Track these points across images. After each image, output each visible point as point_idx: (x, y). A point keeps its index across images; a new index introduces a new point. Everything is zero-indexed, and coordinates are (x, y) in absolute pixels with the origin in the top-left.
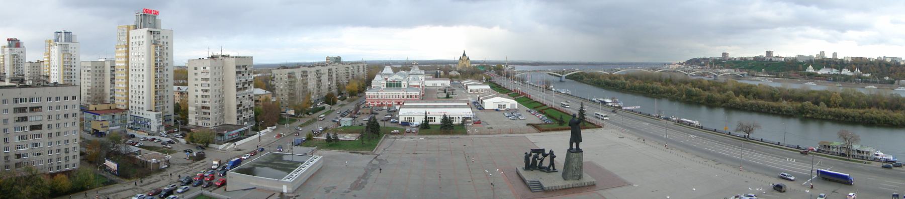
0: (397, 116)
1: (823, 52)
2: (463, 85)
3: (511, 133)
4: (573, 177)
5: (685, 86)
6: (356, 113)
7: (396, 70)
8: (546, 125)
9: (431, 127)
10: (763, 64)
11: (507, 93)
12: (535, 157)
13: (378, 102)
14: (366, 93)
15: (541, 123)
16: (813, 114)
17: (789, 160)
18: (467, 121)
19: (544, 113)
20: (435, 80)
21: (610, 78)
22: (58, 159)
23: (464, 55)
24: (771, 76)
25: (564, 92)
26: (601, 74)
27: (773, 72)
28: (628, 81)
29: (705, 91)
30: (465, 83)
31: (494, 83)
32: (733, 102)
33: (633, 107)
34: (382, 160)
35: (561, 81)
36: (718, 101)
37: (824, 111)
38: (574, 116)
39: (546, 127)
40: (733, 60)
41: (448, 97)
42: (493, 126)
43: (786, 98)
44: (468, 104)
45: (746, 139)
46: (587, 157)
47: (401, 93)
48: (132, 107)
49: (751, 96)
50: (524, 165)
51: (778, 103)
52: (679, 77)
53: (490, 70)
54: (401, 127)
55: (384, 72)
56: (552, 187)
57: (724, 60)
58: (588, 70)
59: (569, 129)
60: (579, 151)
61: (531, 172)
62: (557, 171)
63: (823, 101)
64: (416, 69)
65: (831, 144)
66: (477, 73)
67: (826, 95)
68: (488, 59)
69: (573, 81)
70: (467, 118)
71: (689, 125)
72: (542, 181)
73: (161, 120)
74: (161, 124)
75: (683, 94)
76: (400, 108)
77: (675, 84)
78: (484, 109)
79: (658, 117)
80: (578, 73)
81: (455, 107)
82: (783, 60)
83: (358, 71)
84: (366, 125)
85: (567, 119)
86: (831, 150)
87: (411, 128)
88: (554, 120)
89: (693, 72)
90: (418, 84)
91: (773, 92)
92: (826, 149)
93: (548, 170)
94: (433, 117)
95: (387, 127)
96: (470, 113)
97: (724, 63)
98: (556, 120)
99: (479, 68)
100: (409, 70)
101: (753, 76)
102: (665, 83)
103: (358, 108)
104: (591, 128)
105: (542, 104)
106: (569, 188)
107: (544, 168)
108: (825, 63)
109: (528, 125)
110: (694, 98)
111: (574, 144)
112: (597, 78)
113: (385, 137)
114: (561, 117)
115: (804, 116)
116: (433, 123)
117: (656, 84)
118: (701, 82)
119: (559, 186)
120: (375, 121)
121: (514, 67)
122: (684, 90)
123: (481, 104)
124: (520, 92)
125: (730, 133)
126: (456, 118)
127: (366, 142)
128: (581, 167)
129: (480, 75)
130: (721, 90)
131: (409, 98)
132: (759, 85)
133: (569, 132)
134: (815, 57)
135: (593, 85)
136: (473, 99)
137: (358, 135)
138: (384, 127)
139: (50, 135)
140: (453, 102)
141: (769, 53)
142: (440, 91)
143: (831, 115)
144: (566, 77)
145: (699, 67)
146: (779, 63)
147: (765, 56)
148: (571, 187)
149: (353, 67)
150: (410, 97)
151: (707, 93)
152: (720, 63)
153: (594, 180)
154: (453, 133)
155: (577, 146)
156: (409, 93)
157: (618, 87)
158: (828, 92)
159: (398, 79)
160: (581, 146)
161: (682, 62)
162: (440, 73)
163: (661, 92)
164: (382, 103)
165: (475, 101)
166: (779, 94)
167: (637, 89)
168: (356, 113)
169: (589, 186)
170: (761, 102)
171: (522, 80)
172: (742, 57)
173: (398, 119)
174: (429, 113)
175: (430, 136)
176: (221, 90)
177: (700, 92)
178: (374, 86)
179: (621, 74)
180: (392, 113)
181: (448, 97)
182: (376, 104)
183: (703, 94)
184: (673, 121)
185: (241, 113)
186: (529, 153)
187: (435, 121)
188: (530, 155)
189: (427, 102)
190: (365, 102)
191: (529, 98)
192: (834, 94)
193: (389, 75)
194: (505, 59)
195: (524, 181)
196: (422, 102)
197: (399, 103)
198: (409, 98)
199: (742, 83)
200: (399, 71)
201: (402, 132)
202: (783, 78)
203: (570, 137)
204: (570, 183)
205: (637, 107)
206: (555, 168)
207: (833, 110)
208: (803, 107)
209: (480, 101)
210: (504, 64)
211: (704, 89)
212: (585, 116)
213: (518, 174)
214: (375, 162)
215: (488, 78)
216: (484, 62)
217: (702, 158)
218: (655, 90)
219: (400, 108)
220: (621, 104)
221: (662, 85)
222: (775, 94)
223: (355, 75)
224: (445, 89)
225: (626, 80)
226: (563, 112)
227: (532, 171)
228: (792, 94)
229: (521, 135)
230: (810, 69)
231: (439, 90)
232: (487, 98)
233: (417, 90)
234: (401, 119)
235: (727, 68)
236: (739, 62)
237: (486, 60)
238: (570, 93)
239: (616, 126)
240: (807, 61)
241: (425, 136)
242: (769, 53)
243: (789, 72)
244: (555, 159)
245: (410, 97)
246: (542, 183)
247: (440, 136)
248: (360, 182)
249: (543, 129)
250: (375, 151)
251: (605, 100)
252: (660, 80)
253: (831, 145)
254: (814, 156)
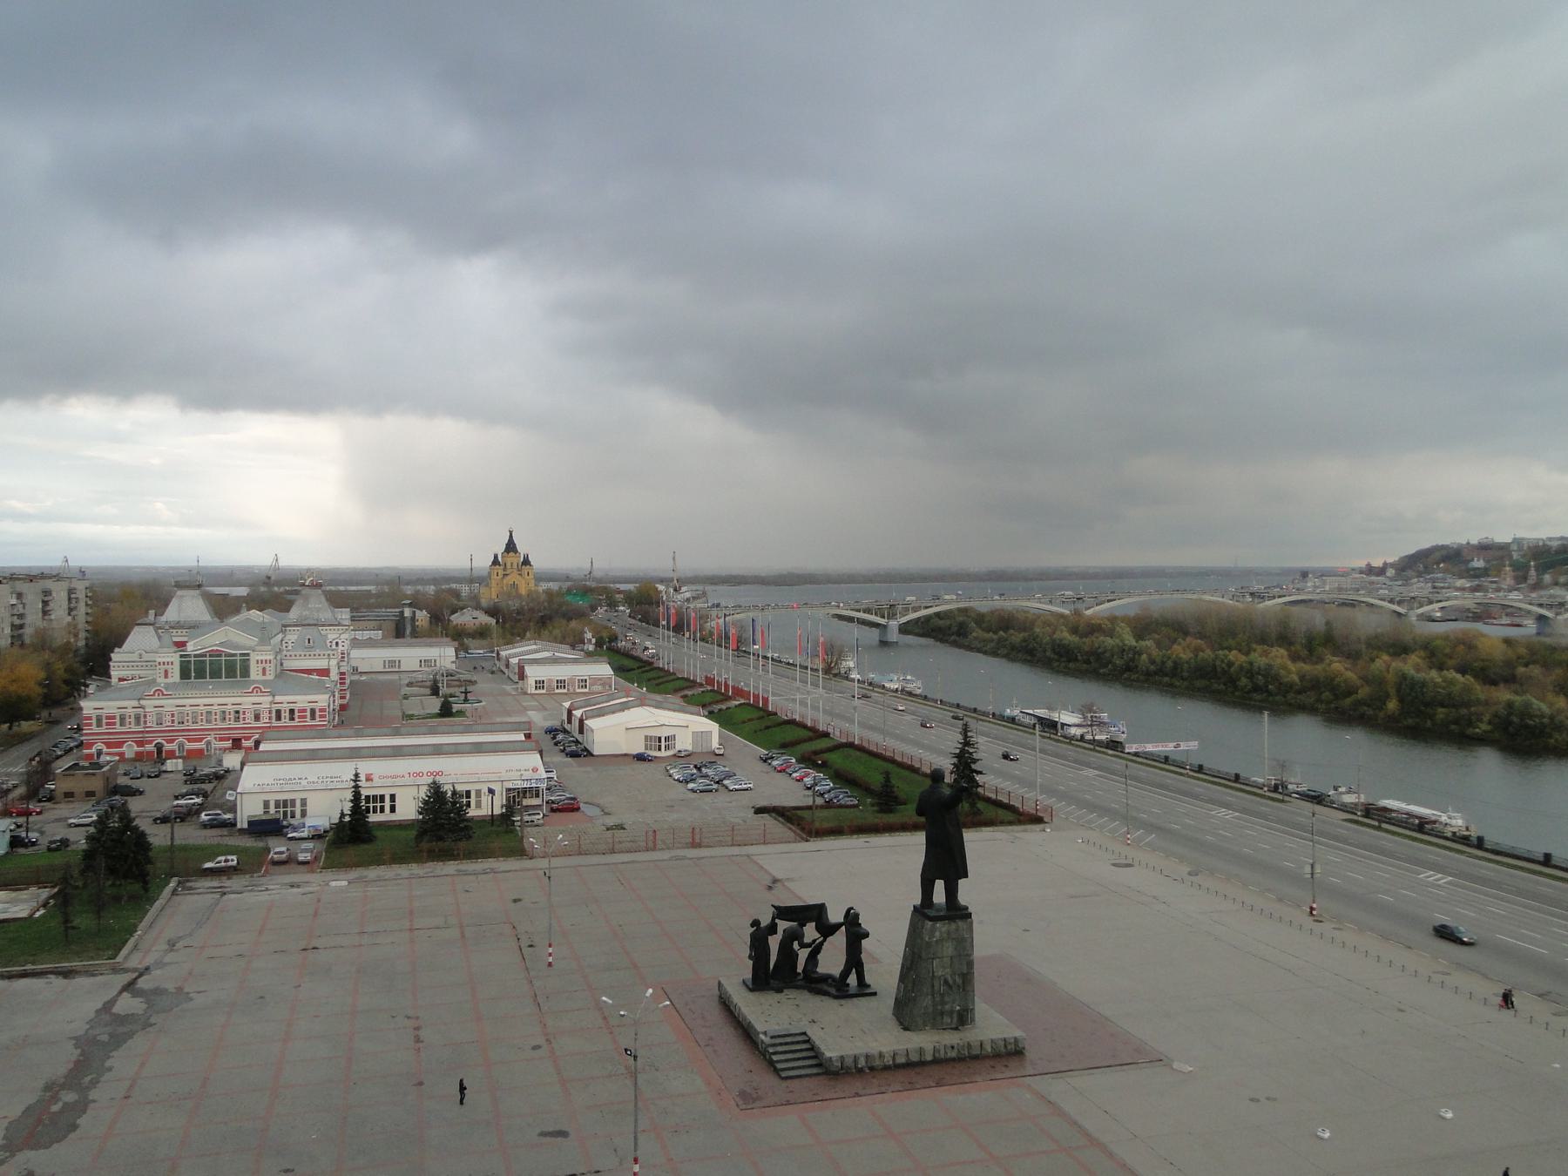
0: (230, 796)
2: (507, 666)
4: (935, 1020)
5: (1397, 664)
6: (32, 794)
7: (223, 608)
8: (825, 813)
9: (378, 833)
12: (793, 936)
13: (140, 743)
14: (83, 703)
15: (809, 802)
18: (526, 802)
19: (823, 767)
20: (392, 646)
23: (511, 547)
25: (894, 686)
26: (1039, 616)
30: (515, 656)
34: (158, 992)
35: (884, 643)
38: (937, 776)
39: (823, 819)
41: (446, 711)
42: (627, 818)
44: (528, 736)
46: (987, 939)
47: (247, 702)
50: (746, 970)
52: (1366, 624)
54: (249, 842)
55: (171, 614)
56: (856, 1059)
58: (987, 602)
59: (915, 828)
60: (957, 912)
61: (778, 996)
64: (316, 606)
69: (930, 641)
70: (524, 792)
75: (1388, 696)
76: (243, 764)
78: (590, 754)
80: (950, 611)
81: (478, 749)
83: (45, 613)
84: (83, 844)
87: (292, 845)
89: (1431, 602)
90: (320, 664)
93: (835, 988)
94: (387, 793)
95: (185, 848)
96: (535, 770)
99: (569, 598)
100: (285, 607)
102: (1304, 653)
103: (41, 773)
104: (1002, 823)
107: (826, 978)
109: (759, 811)
110: (1441, 713)
111: (939, 886)
112: (1025, 630)
113: (174, 892)
116: (387, 816)
117: (1265, 653)
118: (1471, 647)
119: (881, 1055)
120: (126, 819)
121: (704, 594)
122: (1390, 677)
123: (576, 734)
126: (478, 793)
127: (83, 921)
129: (573, 624)
131: (285, 721)
133: (920, 839)
135: (1006, 656)
136: (545, 719)
137: (45, 893)
138: (172, 848)
140: (468, 730)
142: (415, 690)
144: (905, 629)
145: (1460, 583)
148: (929, 1058)
149: (20, 596)
151: (1504, 695)
153: (1018, 1033)
154: (471, 855)
155: (951, 892)
156: (285, 701)
157: (1106, 666)
159: (237, 647)
160: (967, 892)
162: (413, 618)
163: (1286, 688)
164: (159, 747)
165: (555, 723)
167: (1185, 674)
168: (32, 794)
169: (997, 1056)
171: (739, 645)
173: (232, 808)
174: (369, 779)
175: (373, 873)
178: (123, 674)
180: (208, 787)
181: (446, 711)
182: (130, 750)
183: (1482, 697)
184: (1344, 808)
186: (765, 922)
187: (393, 809)
188: (772, 929)
189: (358, 735)
190: (80, 745)
193: (193, 627)
195: (746, 1032)
196: (339, 737)
197: (236, 744)
198: (285, 721)
200: (237, 611)
201: (252, 864)
203: (922, 859)
204: (925, 1041)
205: (1183, 746)
206: (868, 979)
209: (576, 723)
211: (1488, 674)
212: (978, 778)
213: (726, 1004)
214: (127, 1004)
215: (605, 634)
217: (1485, 976)
218: (1260, 680)
219: (243, 764)
220: (1120, 732)
221: (1295, 658)
223: (28, 632)
224: (435, 682)
225: (1139, 636)
226: (892, 761)
227: (779, 991)
229: (735, 850)
231: (410, 684)
232: (601, 713)
233: (320, 688)
234: (249, 809)
238: (916, 686)
239: (1092, 812)
241: (355, 873)
244: (864, 942)
246: (814, 1037)
247: (415, 869)
248: (55, 1108)
249: (817, 825)
250: (126, 958)
251: (1055, 716)
252: (1284, 639)
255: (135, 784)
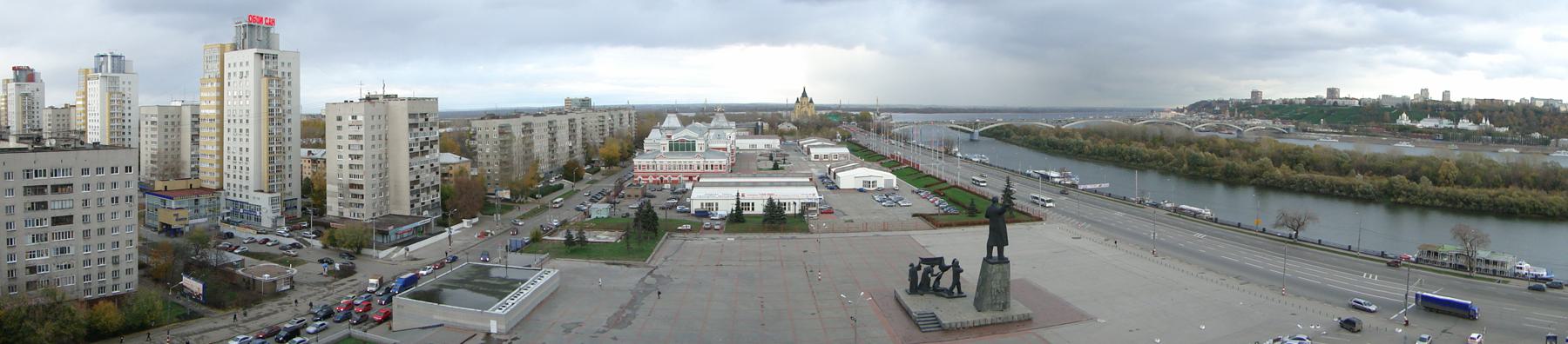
0: (688, 200)
1: (1426, 90)
2: (802, 148)
3: (885, 230)
4: (992, 306)
5: (1187, 149)
6: (617, 195)
7: (686, 122)
8: (947, 217)
9: (746, 219)
10: (1322, 111)
11: (878, 160)
12: (928, 271)
13: (654, 177)
14: (634, 160)
15: (937, 212)
16: (1408, 196)
17: (1368, 276)
18: (810, 209)
19: (943, 196)
20: (753, 138)
21: (1057, 135)
22: (101, 275)
23: (804, 95)
24: (1336, 131)
25: (977, 160)
26: (1041, 129)
27: (1339, 125)
28: (1088, 141)
29: (1222, 157)
30: (805, 143)
31: (856, 144)
32: (1270, 176)
33: (1098, 186)
34: (661, 276)
35: (972, 140)
36: (1243, 174)
37: (1428, 192)
38: (995, 200)
39: (945, 219)
40: (1271, 103)
41: (776, 167)
42: (854, 217)
43: (1363, 169)
44: (811, 180)
45: (1293, 240)
46: (1016, 271)
47: (695, 161)
48: (229, 185)
49: (1301, 165)
50: (907, 286)
51: (1347, 177)
52: (1177, 133)
53: (849, 121)
54: (695, 219)
55: (665, 124)
56: (956, 324)
57: (1254, 104)
58: (1019, 121)
59: (985, 223)
60: (1003, 260)
61: (920, 297)
62: (965, 296)
63: (1427, 174)
64: (721, 120)
65: (1440, 250)
66: (827, 126)
67: (1432, 165)
68: (845, 102)
69: (994, 139)
70: (809, 204)
71: (1195, 216)
72: (938, 314)
73: (279, 207)
74: (279, 214)
75: (1184, 162)
76: (693, 187)
77: (1169, 146)
78: (838, 188)
79: (1140, 203)
80: (1002, 126)
81: (789, 184)
82: (1357, 103)
83: (621, 123)
84: (634, 216)
85: (982, 206)
86: (1439, 260)
87: (713, 222)
88: (959, 208)
89: (1200, 124)
90: (724, 146)
91: (1340, 159)
92: (1432, 258)
93: (949, 294)
94: (751, 202)
95: (671, 220)
96: (814, 195)
97: (1254, 108)
98: (964, 207)
99: (830, 118)
100: (709, 121)
101: (1305, 131)
102: (1152, 144)
103: (619, 187)
104: (1024, 221)
105: (939, 179)
106: (986, 325)
107: (943, 290)
108: (1430, 109)
109: (915, 215)
110: (1203, 169)
111: (995, 249)
112: (1034, 135)
113: (667, 237)
114: (973, 202)
115: (1392, 200)
116: (750, 212)
117: (1136, 145)
118: (1215, 142)
119: (968, 322)
120: (650, 208)
121: (891, 116)
122: (1185, 155)
123: (833, 180)
124: (900, 159)
125: (1264, 229)
126: (789, 203)
127: (634, 246)
128: (1007, 289)
129: (832, 130)
130: (1250, 155)
131: (709, 170)
132: (1315, 146)
133: (987, 228)
134: (1412, 98)
135: (1027, 147)
136: (819, 172)
137: (621, 233)
138: (666, 220)
139: (86, 234)
140: (785, 176)
141: (1332, 92)
142: (763, 158)
143: (1441, 199)
144: (981, 134)
145: (1211, 116)
146: (1349, 109)
147: (1325, 96)
148: (989, 323)
149: (612, 117)
150: (710, 167)
151: (1225, 161)
152: (1247, 109)
153: (1029, 311)
154: (786, 230)
155: (1000, 252)
156: (709, 161)
157: (1070, 151)
158: (1435, 159)
159: (690, 137)
160: (1007, 252)
161: (1181, 107)
162: (762, 126)
163: (1145, 160)
164: (662, 179)
165: (823, 174)
166: (1350, 163)
167: (1104, 154)
168: (617, 195)
169: (1020, 321)
170: (1318, 176)
171: (905, 139)
172: (1285, 99)
173: (689, 206)
174: (743, 196)
175: (744, 236)
176: (383, 156)
177: (1213, 159)
178: (649, 148)
179: (1076, 127)
180: (680, 196)
181: (776, 167)
182: (651, 179)
183: (1218, 162)
184: (1167, 209)
185: (418, 196)
186: (916, 265)
187: (753, 209)
188: (919, 268)
189: (739, 177)
190: (633, 177)
191: (917, 170)
192: (1446, 162)
193: (674, 129)
194: (875, 103)
195: (907, 312)
196: (731, 177)
197: (691, 178)
198: (709, 170)
199: (1285, 144)
200: (691, 123)
201: (696, 229)
202: (1356, 134)
203: (987, 237)
204: (987, 316)
205: (1103, 185)
206: (962, 290)
207: (1443, 189)
208: (1391, 185)
209: (832, 174)
210: (874, 110)
211: (1220, 154)
212: (1013, 201)
213: (898, 300)
214: (649, 280)
215: (846, 134)
216: (839, 107)
217: (1217, 273)
218: (1134, 156)
219: (693, 187)
220: (1076, 180)
221: (1148, 147)
222: (1342, 162)
223: (615, 130)
224: (771, 154)
225: (1084, 139)
226: (976, 194)
227: (922, 295)
228: (1372, 163)
229: (903, 233)
230: (1404, 120)
231: (761, 155)
232: (843, 170)
233: (723, 156)
234: (696, 206)
235: (1260, 117)
236: (1280, 107)
237: (842, 103)
238: (987, 160)
240: (1398, 105)
241: (737, 235)
242: (1332, 92)
243: (1368, 124)
244: (961, 274)
245: (710, 167)
246: (938, 316)
247: (762, 235)
248: (624, 315)
249: (940, 223)
250: (650, 261)
251: (1048, 173)
252: (1144, 139)
253: (1440, 251)
254: (1411, 269)
255: (652, 193)
